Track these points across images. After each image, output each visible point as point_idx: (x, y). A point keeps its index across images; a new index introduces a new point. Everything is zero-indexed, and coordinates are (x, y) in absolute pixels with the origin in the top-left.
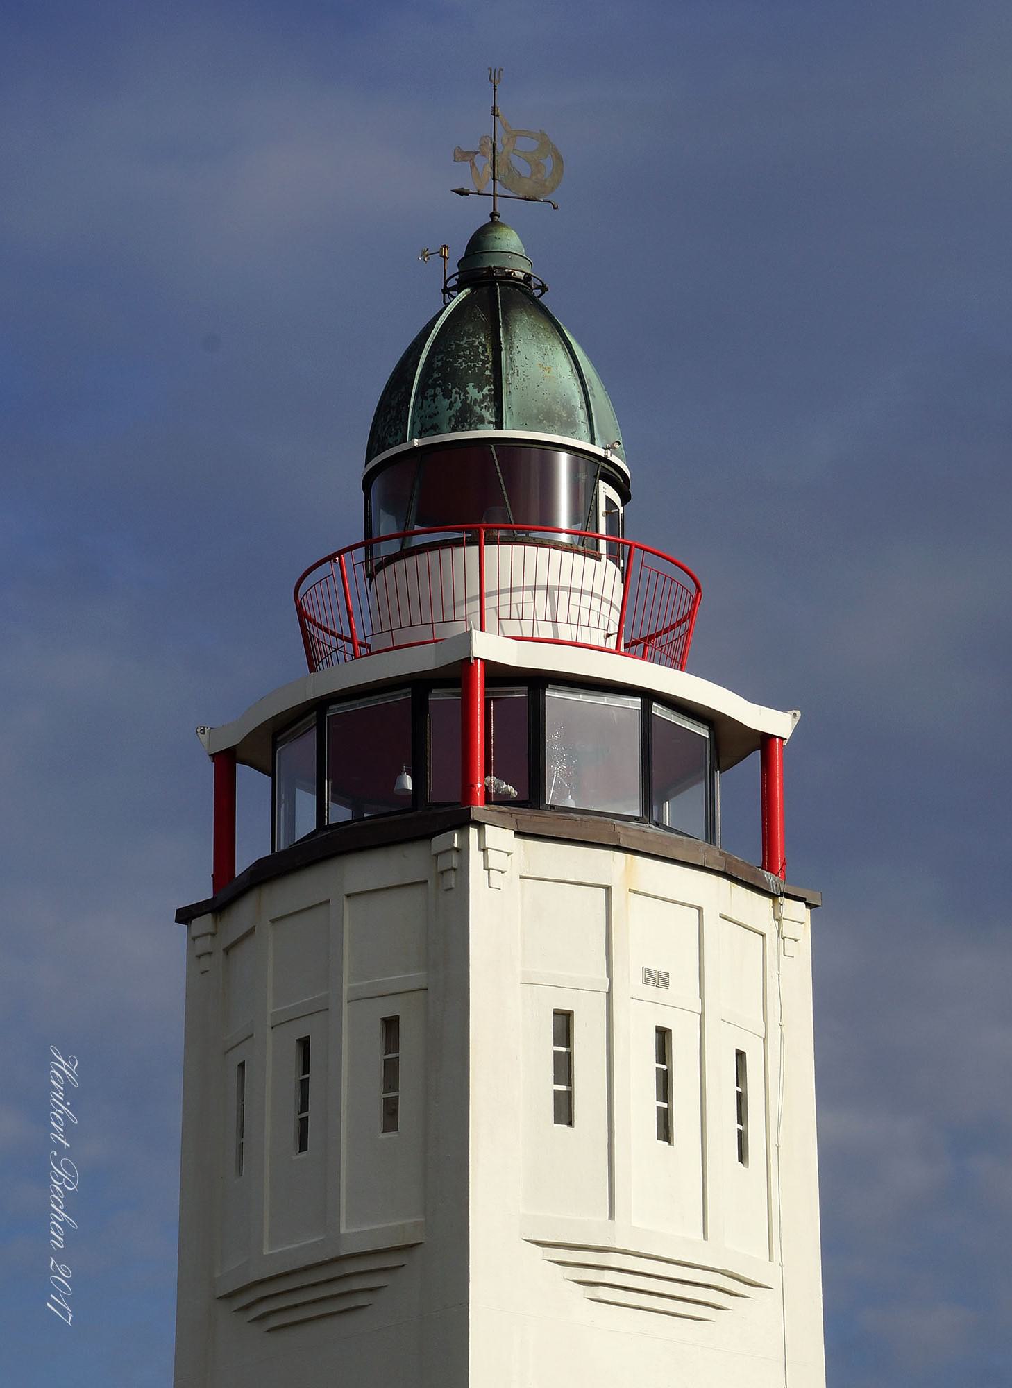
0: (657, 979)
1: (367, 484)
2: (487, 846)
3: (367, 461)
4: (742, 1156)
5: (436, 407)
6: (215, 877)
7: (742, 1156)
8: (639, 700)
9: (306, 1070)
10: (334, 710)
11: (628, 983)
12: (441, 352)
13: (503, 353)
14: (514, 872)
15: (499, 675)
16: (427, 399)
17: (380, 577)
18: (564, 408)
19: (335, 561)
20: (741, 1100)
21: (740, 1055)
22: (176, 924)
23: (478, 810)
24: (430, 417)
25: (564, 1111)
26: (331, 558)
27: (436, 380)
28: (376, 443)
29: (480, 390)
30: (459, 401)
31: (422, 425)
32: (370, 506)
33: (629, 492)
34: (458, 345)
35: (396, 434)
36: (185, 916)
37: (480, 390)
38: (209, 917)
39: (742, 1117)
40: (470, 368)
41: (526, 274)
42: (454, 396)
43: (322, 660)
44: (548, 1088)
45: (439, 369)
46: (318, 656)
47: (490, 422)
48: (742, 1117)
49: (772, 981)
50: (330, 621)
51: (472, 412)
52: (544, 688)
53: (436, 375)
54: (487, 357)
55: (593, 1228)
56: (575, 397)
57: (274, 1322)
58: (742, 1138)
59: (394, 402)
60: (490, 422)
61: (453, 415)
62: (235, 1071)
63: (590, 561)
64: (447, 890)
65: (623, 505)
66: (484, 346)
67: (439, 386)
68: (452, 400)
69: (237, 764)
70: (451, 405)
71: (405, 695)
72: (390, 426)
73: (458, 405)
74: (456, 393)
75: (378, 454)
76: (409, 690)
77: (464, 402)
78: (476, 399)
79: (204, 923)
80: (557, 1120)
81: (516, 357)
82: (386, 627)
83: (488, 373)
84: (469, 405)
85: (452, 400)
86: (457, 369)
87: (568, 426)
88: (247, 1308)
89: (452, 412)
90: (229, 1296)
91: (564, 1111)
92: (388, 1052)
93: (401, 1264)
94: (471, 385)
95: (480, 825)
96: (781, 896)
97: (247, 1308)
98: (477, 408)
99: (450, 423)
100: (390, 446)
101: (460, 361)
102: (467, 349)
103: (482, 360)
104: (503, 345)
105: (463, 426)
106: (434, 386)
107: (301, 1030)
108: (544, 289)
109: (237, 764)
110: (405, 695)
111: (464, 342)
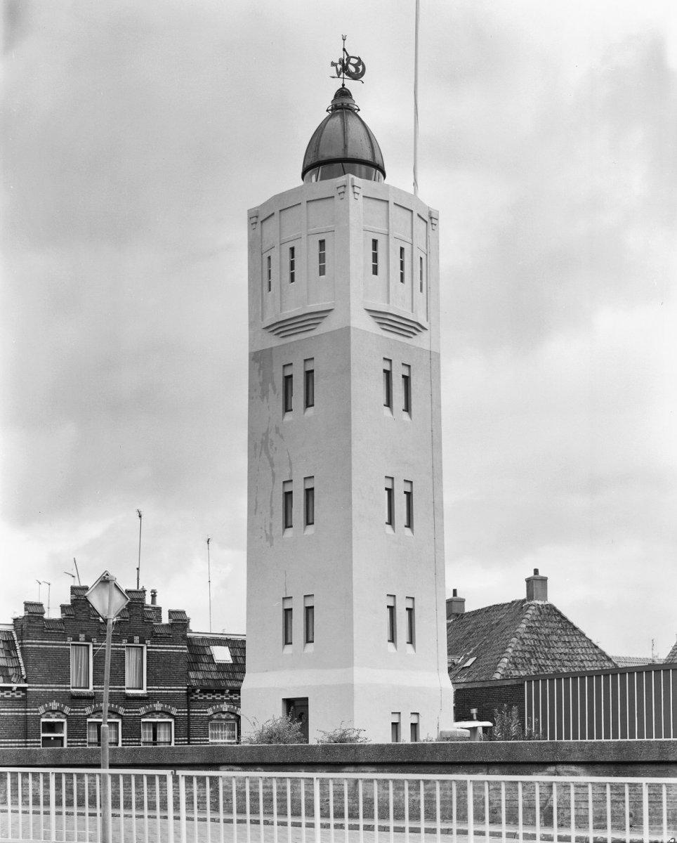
4: (402, 280)
7: (402, 280)
9: (293, 257)
14: (361, 194)
20: (402, 263)
21: (421, 258)
22: (326, 273)
25: (375, 271)
39: (402, 268)
44: (370, 263)
46: (202, 740)
48: (402, 268)
57: (282, 335)
58: (402, 275)
62: (266, 260)
88: (273, 331)
90: (268, 328)
91: (375, 271)
93: (271, 214)
97: (273, 331)
107: (291, 245)
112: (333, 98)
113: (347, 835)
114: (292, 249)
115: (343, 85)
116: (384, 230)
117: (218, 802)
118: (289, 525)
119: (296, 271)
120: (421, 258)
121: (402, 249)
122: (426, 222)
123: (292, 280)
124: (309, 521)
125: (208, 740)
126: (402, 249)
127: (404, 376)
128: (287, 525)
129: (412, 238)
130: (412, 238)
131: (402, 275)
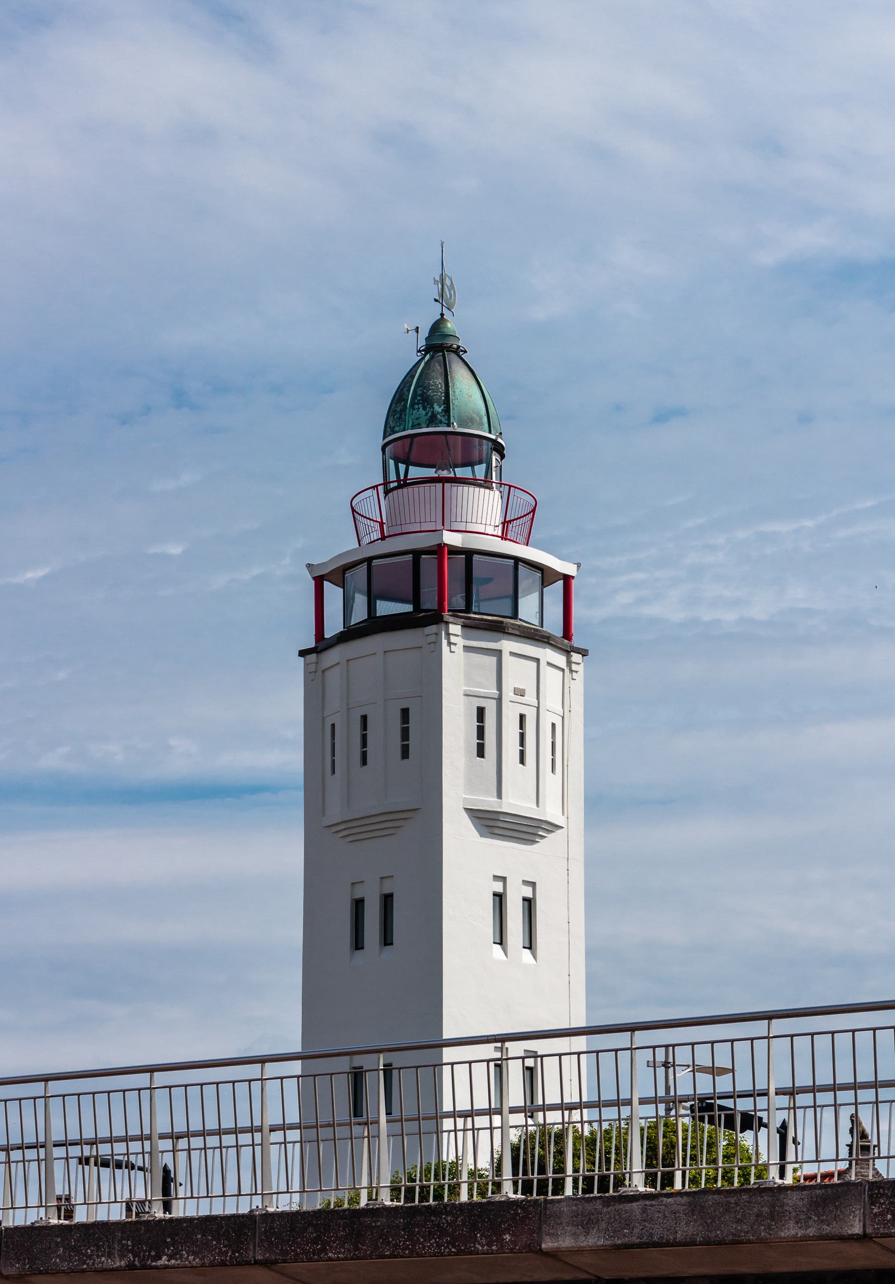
0: (520, 692)
1: (383, 449)
2: (450, 632)
3: (384, 439)
5: (419, 414)
6: (316, 635)
8: (410, 466)
10: (375, 562)
11: (508, 694)
12: (421, 386)
13: (450, 388)
15: (454, 551)
16: (415, 410)
17: (390, 495)
18: (478, 416)
19: (374, 489)
21: (553, 725)
23: (447, 616)
24: (417, 419)
25: (481, 753)
26: (373, 487)
27: (419, 400)
28: (388, 429)
29: (440, 407)
30: (430, 412)
31: (413, 423)
32: (385, 458)
33: (504, 453)
34: (429, 383)
35: (400, 426)
36: (303, 653)
37: (440, 407)
38: (314, 655)
40: (435, 395)
41: (458, 345)
42: (428, 409)
43: (365, 536)
45: (420, 395)
47: (445, 423)
49: (566, 691)
50: (367, 514)
51: (436, 418)
52: (473, 555)
53: (419, 398)
54: (442, 390)
55: (489, 802)
56: (482, 410)
58: (522, 754)
59: (398, 409)
60: (445, 423)
61: (427, 419)
63: (487, 491)
64: (431, 652)
65: (501, 461)
66: (441, 384)
67: (421, 403)
68: (427, 411)
69: (324, 582)
70: (426, 414)
71: (409, 557)
72: (397, 421)
73: (430, 414)
74: (429, 408)
75: (390, 435)
76: (411, 555)
77: (433, 412)
78: (438, 412)
79: (312, 657)
80: (478, 756)
81: (456, 390)
82: (399, 523)
83: (443, 398)
84: (435, 414)
85: (427, 411)
86: (429, 396)
87: (480, 426)
88: (337, 832)
89: (427, 417)
91: (481, 753)
92: (403, 724)
94: (436, 404)
95: (447, 623)
96: (572, 651)
97: (337, 832)
98: (438, 416)
99: (426, 422)
100: (397, 432)
101: (430, 392)
102: (433, 386)
103: (440, 392)
104: (450, 385)
105: (432, 424)
106: (418, 404)
108: (465, 352)
109: (324, 582)
110: (409, 557)
111: (432, 381)
112: (427, 336)
113: (319, 1196)
114: (364, 718)
115: (442, 315)
116: (494, 692)
117: (524, 1144)
118: (360, 947)
119: (369, 749)
120: (553, 725)
121: (522, 717)
122: (563, 670)
123: (364, 762)
124: (387, 940)
125: (875, 1146)
126: (522, 717)
127: (524, 899)
128: (358, 943)
129: (538, 698)
130: (538, 698)
131: (522, 754)
